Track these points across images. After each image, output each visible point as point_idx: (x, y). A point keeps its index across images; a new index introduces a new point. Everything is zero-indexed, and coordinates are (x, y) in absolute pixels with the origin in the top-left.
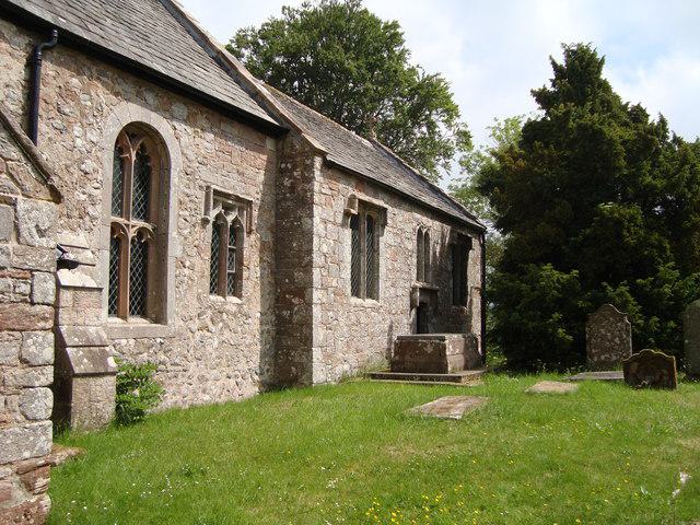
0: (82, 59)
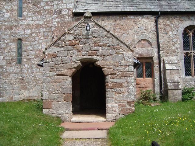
0: (169, 16)
